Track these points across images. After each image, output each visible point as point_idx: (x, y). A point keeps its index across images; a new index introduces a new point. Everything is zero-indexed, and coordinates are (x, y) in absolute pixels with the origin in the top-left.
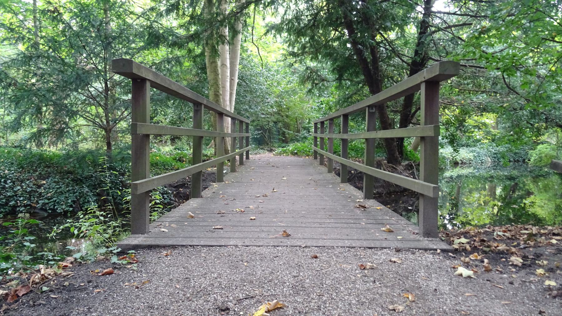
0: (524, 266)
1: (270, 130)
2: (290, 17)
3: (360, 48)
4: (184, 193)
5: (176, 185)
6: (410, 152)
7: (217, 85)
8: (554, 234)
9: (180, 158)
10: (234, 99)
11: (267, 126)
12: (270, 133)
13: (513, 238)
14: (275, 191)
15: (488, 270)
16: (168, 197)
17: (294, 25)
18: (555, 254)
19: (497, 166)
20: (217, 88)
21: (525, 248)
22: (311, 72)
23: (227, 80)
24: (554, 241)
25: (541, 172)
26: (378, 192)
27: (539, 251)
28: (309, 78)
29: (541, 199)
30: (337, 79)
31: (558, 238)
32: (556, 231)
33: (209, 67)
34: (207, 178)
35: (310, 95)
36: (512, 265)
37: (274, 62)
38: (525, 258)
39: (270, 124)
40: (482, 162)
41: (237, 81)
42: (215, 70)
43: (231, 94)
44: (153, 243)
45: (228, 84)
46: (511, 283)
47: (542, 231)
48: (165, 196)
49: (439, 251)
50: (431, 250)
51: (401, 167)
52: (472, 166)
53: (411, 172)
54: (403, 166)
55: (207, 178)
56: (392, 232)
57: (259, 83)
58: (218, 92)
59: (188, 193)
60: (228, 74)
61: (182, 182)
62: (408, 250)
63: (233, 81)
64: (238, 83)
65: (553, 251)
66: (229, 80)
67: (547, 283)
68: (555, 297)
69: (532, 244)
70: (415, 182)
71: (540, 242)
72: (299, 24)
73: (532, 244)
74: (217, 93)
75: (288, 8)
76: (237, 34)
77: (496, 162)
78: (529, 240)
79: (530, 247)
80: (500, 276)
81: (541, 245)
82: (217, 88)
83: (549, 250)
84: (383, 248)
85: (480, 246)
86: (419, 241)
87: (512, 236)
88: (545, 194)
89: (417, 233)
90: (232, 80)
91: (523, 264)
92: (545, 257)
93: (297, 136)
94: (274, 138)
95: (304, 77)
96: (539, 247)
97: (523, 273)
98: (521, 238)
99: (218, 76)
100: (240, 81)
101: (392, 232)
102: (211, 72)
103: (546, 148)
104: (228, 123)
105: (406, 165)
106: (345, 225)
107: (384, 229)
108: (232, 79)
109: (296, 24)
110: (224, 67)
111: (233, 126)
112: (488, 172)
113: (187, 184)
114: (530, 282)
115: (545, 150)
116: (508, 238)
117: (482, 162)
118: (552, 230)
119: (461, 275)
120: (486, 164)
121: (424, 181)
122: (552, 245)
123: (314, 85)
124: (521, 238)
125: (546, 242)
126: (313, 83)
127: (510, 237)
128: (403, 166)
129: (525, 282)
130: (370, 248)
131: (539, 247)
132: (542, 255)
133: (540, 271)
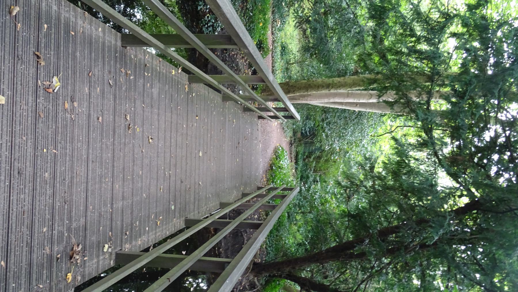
1: (312, 143)
2: (412, 165)
3: (365, 241)
6: (279, 284)
7: (340, 87)
9: (263, 48)
10: (337, 107)
11: (316, 140)
12: (310, 143)
14: (151, 141)
16: (210, 31)
17: (404, 168)
20: (336, 87)
22: (357, 185)
23: (356, 100)
26: (221, 253)
28: (352, 183)
30: (349, 212)
33: (359, 78)
35: (335, 184)
37: (380, 147)
39: (318, 144)
41: (357, 109)
42: (356, 84)
43: (341, 104)
45: (351, 100)
48: (211, 29)
51: (252, 277)
53: (247, 287)
54: (253, 279)
57: (353, 132)
58: (332, 88)
60: (362, 101)
63: (355, 105)
64: (355, 111)
66: (355, 101)
72: (405, 174)
74: (330, 87)
75: (423, 162)
76: (390, 106)
82: (336, 87)
90: (356, 104)
93: (311, 170)
94: (305, 147)
95: (353, 178)
100: (357, 113)
102: (353, 80)
104: (311, 100)
105: (255, 283)
108: (357, 105)
109: (405, 171)
110: (369, 96)
113: (226, 53)
123: (345, 188)
126: (347, 187)
128: (253, 279)
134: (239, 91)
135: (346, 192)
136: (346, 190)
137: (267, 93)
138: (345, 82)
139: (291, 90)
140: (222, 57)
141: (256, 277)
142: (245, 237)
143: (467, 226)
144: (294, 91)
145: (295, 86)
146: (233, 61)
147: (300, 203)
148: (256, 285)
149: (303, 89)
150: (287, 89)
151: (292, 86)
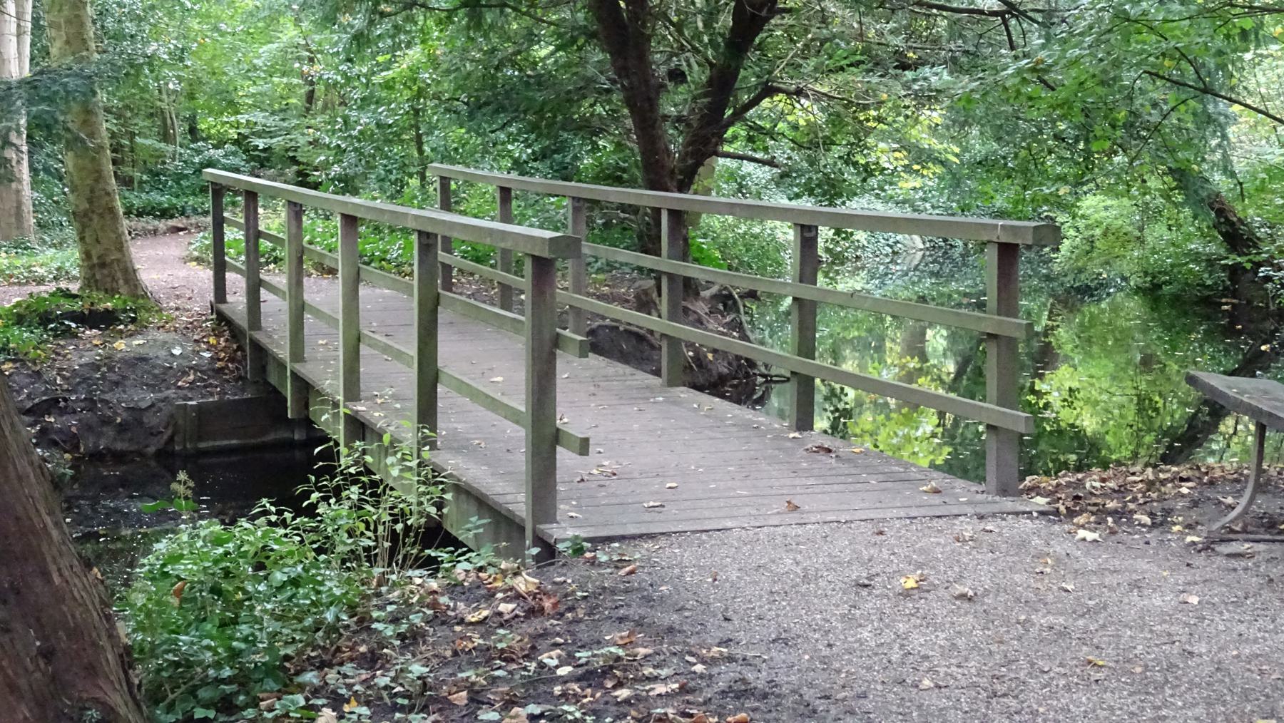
0: (1154, 525)
4: (60, 431)
5: (29, 405)
8: (1182, 480)
13: (1122, 489)
15: (1113, 533)
18: (1190, 508)
19: (941, 264)
21: (1145, 503)
24: (1185, 491)
25: (1083, 277)
27: (1166, 505)
29: (1091, 377)
31: (1190, 484)
32: (1184, 474)
34: (124, 378)
36: (1139, 524)
38: (1152, 515)
40: (894, 253)
44: (645, 531)
46: (1147, 543)
47: (1162, 476)
49: (1035, 514)
50: (1024, 513)
52: (863, 268)
53: (728, 319)
54: (704, 300)
55: (124, 378)
56: (940, 492)
59: (74, 430)
61: (44, 393)
62: (994, 515)
65: (1187, 504)
67: (1189, 539)
68: (1200, 551)
69: (1154, 495)
70: (982, 407)
71: (1165, 494)
73: (1154, 495)
77: (940, 247)
78: (1149, 490)
79: (1152, 501)
80: (1131, 537)
81: (1166, 497)
83: (1180, 504)
84: (957, 516)
85: (1075, 506)
86: (996, 502)
87: (1120, 486)
88: (1104, 361)
89: (983, 492)
91: (1153, 523)
92: (1177, 513)
96: (1165, 500)
97: (1156, 532)
98: (1135, 489)
99: (84, 8)
101: (940, 492)
103: (1106, 208)
106: (841, 487)
107: (925, 488)
111: (294, 222)
112: (913, 283)
113: (65, 400)
114: (1169, 540)
115: (1103, 214)
116: (1114, 491)
117: (894, 253)
118: (1178, 473)
119: (1084, 540)
120: (909, 258)
121: (998, 405)
122: (1183, 496)
124: (1135, 489)
125: (1173, 492)
127: (1117, 488)
128: (704, 300)
129: (1162, 541)
130: (938, 517)
131: (1165, 500)
132: (1172, 510)
133: (1176, 528)
134: (173, 355)
135: (389, 15)
136: (383, 15)
137: (121, 282)
138: (69, 22)
139: (104, 202)
140: (81, 411)
141: (698, 294)
142: (597, 324)
143: (1158, 671)
144: (108, 194)
145: (92, 191)
146: (85, 380)
147: (393, 177)
148: (720, 291)
149: (99, 165)
150: (101, 216)
151: (90, 201)
